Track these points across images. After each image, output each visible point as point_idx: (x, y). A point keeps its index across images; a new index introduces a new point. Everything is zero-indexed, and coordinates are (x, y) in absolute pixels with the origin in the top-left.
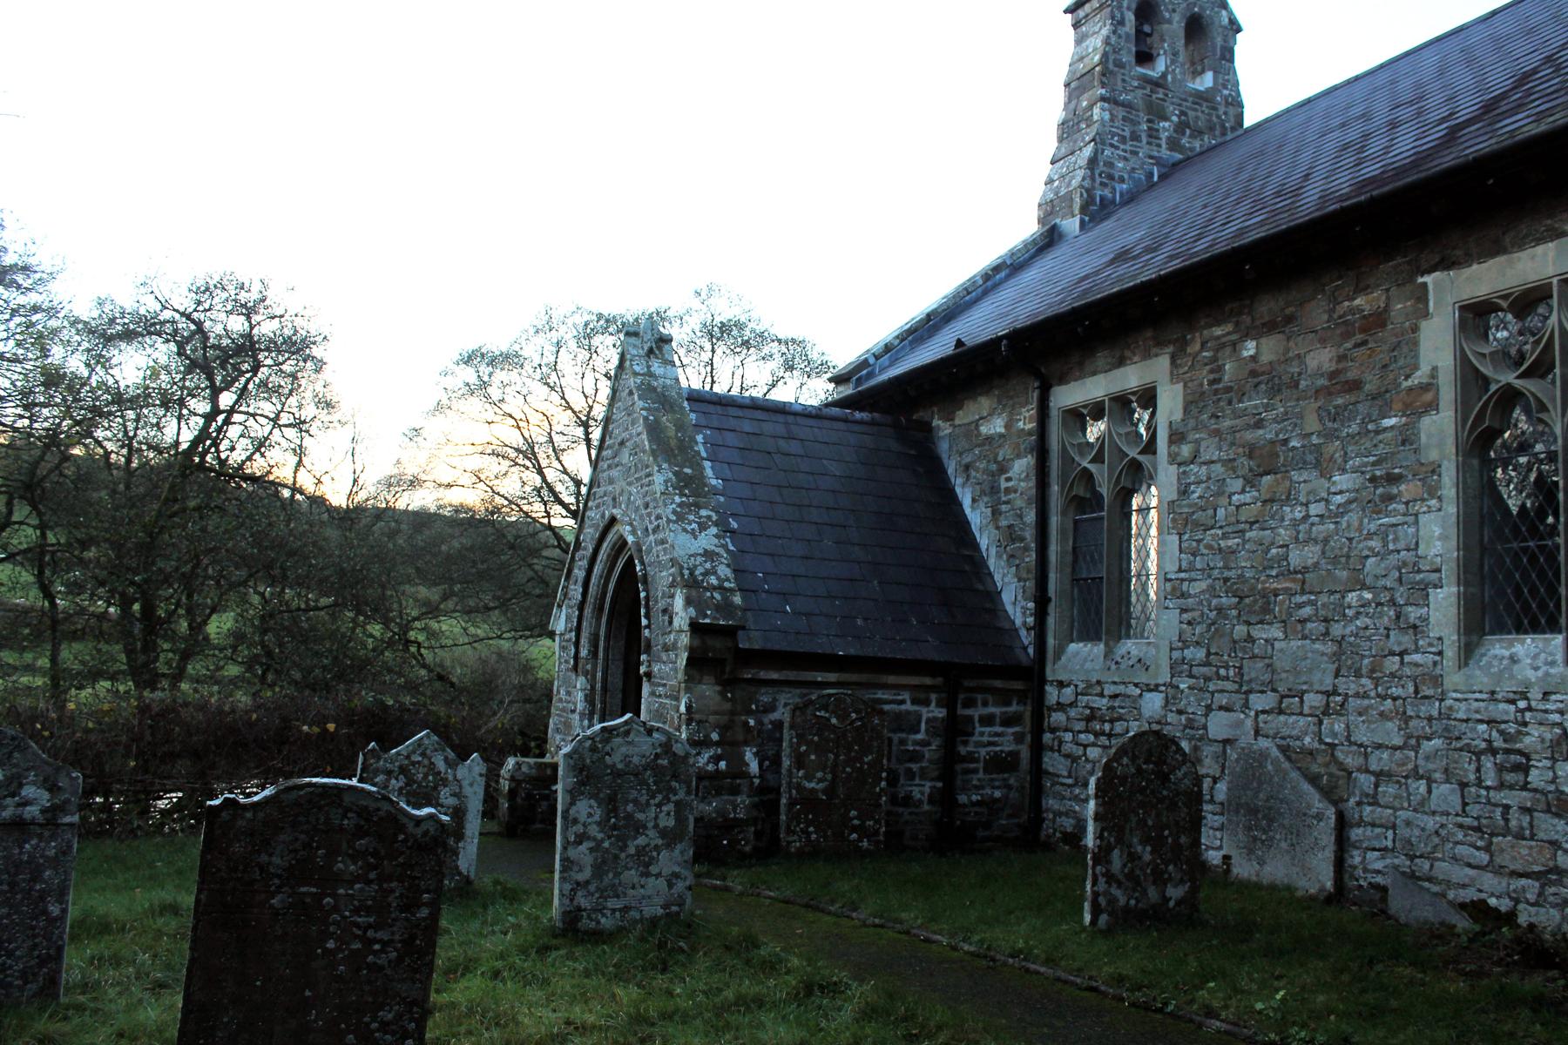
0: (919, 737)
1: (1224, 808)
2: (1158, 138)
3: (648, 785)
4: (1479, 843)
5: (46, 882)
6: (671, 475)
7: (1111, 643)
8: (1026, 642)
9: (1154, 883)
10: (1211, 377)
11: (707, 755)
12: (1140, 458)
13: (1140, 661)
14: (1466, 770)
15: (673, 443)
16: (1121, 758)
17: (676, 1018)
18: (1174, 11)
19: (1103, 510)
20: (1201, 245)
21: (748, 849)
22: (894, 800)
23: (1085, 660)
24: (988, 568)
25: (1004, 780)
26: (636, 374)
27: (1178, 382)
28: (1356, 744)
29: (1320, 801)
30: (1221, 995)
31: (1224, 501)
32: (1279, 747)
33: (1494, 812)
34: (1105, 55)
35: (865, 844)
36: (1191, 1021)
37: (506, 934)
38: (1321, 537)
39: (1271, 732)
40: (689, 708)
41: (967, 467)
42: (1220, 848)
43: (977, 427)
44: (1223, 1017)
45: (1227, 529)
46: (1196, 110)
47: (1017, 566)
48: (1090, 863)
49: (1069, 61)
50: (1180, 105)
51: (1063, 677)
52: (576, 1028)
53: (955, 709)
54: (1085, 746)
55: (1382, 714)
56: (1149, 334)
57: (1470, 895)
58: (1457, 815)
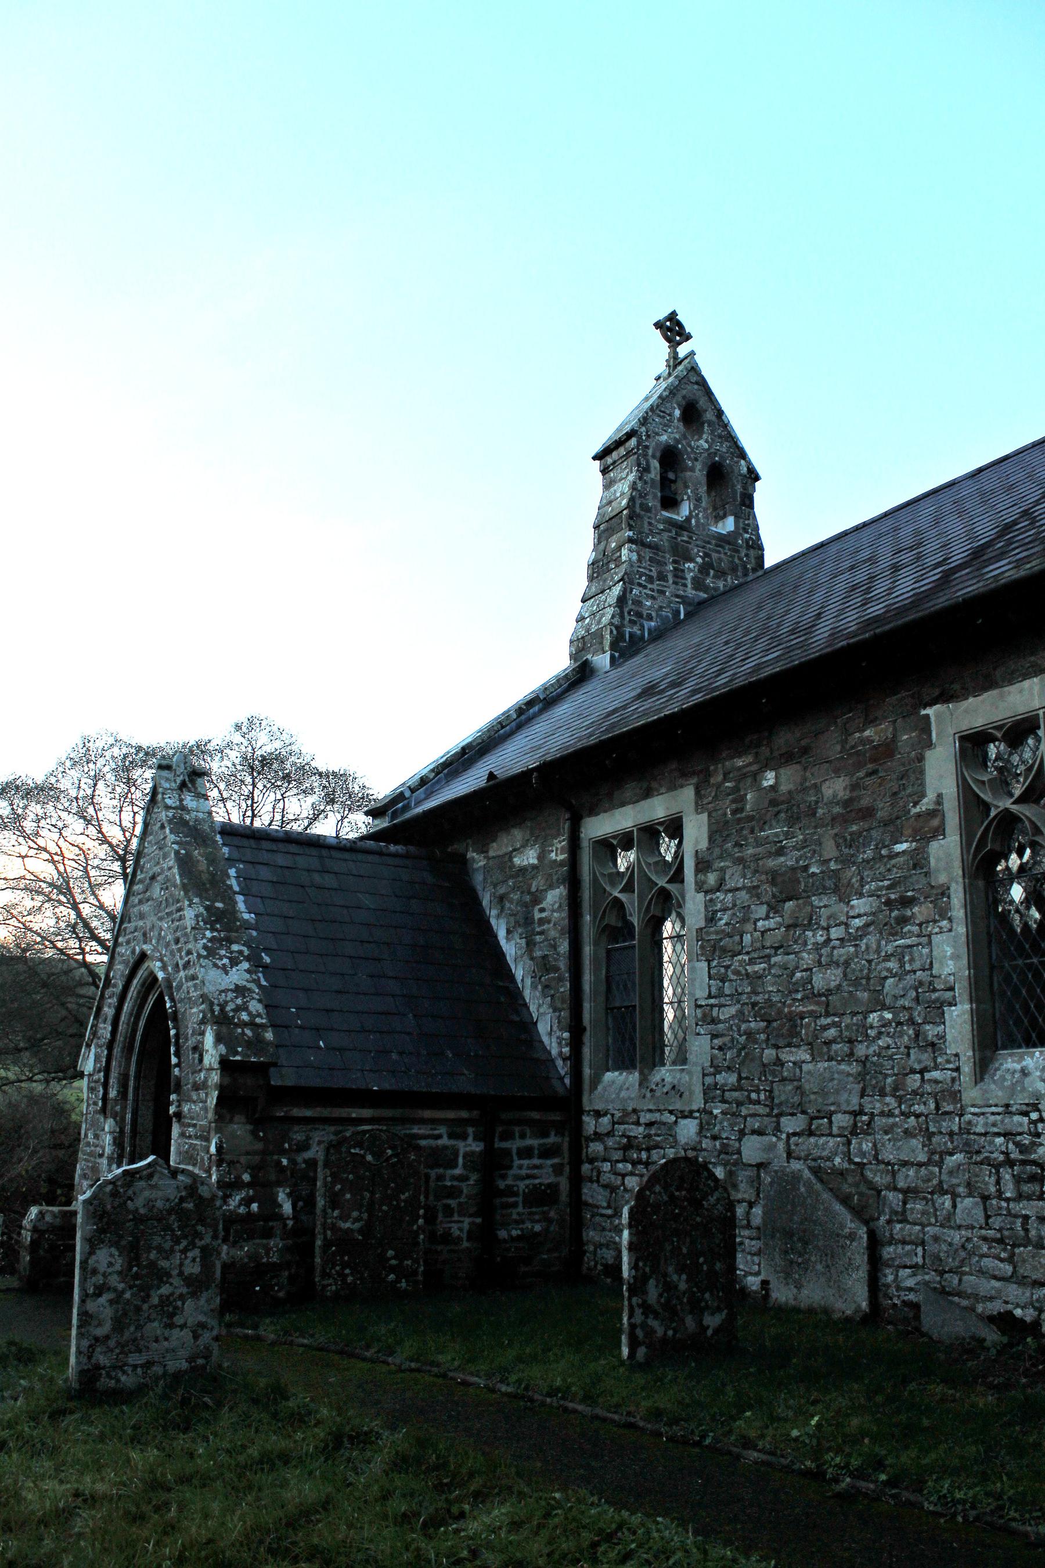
0: (457, 1171)
1: (760, 1233)
2: (686, 579)
3: (173, 1230)
4: (1003, 1255)
6: (202, 909)
7: (646, 1071)
8: (563, 1073)
9: (691, 1313)
10: (734, 806)
11: (238, 1198)
12: (668, 886)
13: (674, 1087)
14: (987, 1184)
15: (205, 877)
16: (653, 1185)
17: (195, 1481)
18: (696, 460)
19: (633, 938)
20: (722, 680)
21: (281, 1294)
22: (432, 1237)
23: (621, 1089)
24: (524, 1000)
25: (544, 1213)
26: (168, 808)
27: (702, 813)
28: (883, 1162)
29: (852, 1221)
30: (757, 1424)
31: (749, 927)
32: (810, 1168)
33: (1014, 1223)
34: (632, 499)
35: (403, 1284)
36: (730, 1453)
37: (16, 1400)
38: (842, 959)
39: (803, 1154)
40: (219, 1149)
41: (501, 899)
42: (758, 1274)
43: (511, 859)
44: (760, 1447)
46: (719, 552)
48: (626, 1294)
49: (598, 504)
50: (703, 547)
51: (599, 1106)
52: (85, 1501)
53: (493, 1143)
54: (624, 1176)
55: (906, 1132)
57: (996, 1307)
58: (981, 1228)
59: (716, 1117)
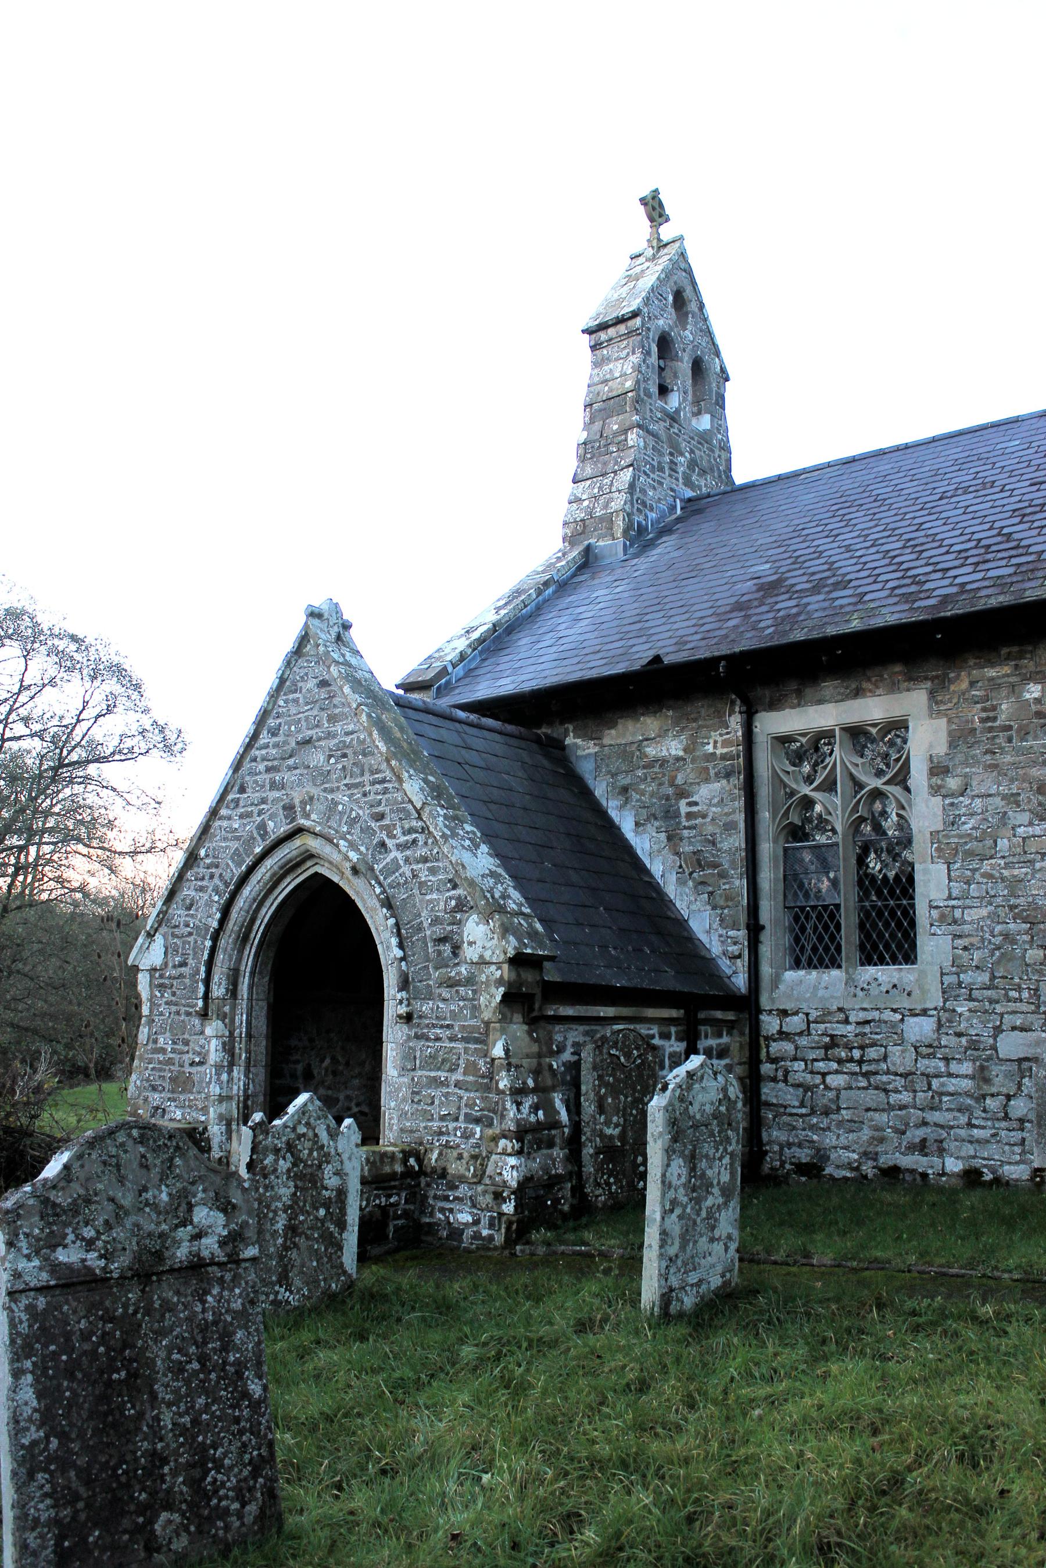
5: (239, 1350)
10: (984, 715)
13: (895, 986)
45: (1011, 859)
47: (711, 894)
49: (587, 381)
54: (824, 1075)
56: (898, 668)
59: (960, 1015)
